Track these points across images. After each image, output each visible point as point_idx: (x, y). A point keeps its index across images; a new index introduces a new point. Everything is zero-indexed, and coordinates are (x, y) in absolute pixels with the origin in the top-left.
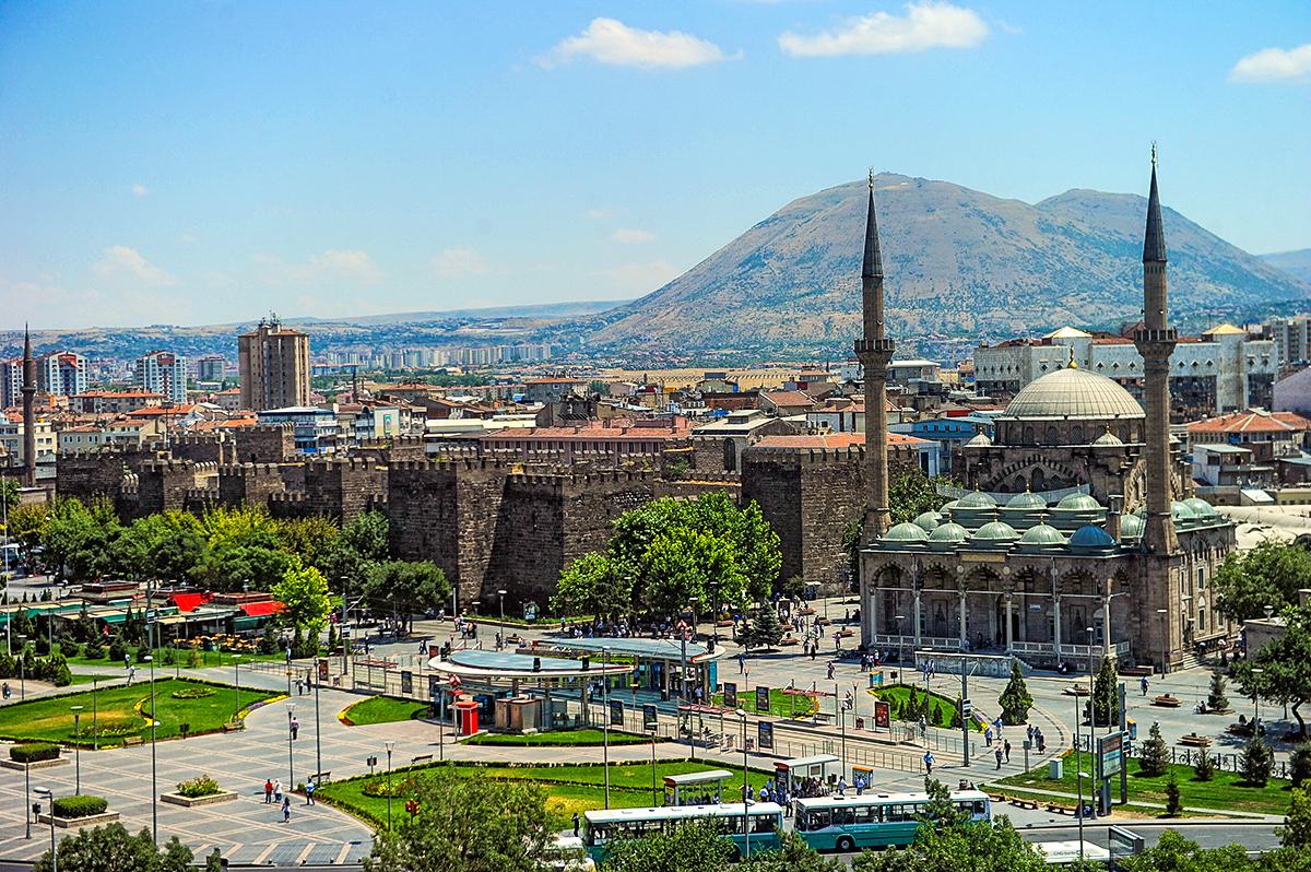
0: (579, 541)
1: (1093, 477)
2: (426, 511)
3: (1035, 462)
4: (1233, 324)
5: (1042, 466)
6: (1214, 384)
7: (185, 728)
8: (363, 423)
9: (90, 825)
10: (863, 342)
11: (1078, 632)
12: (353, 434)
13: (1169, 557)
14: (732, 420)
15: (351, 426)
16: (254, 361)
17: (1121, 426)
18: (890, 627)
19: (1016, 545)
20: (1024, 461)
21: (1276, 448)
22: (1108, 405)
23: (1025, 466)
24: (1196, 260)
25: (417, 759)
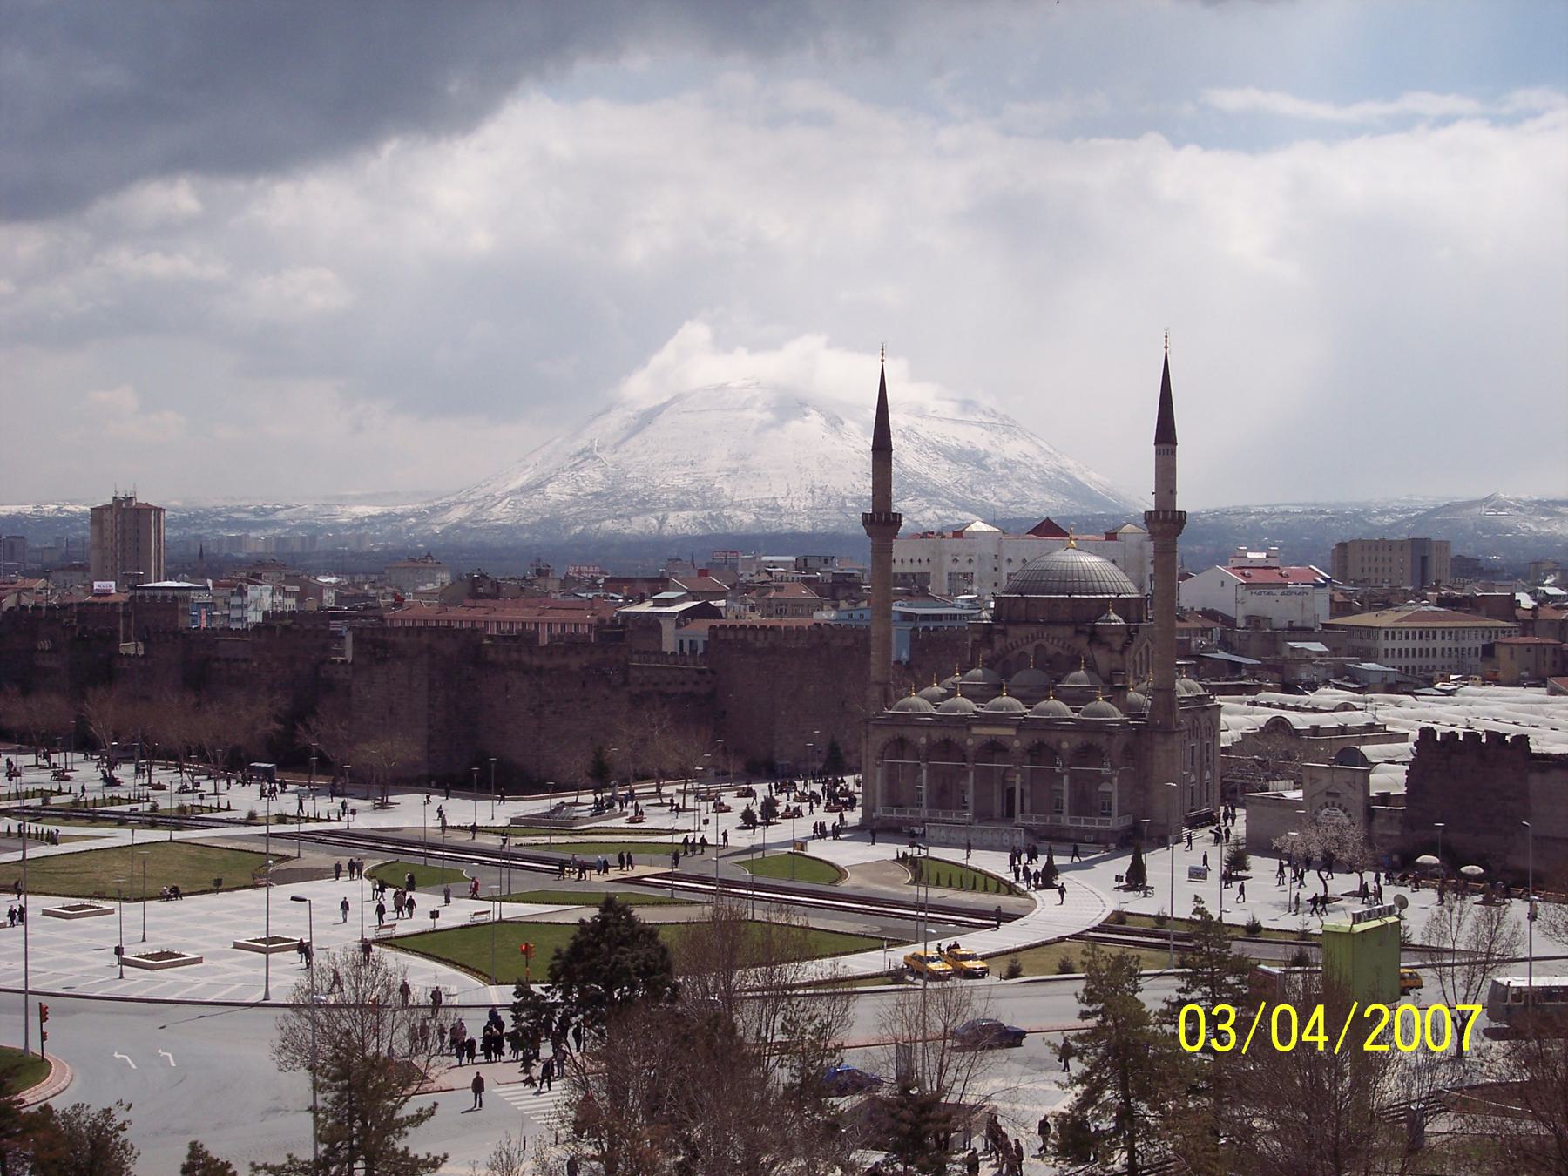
0: (554, 713)
1: (1095, 654)
2: (394, 679)
3: (1038, 638)
4: (523, 639)
5: (1046, 643)
6: (867, 639)
7: (218, 882)
8: (236, 600)
9: (1480, 651)
10: (242, 619)
11: (1085, 803)
12: (227, 612)
13: (1175, 732)
14: (659, 603)
15: (225, 603)
16: (107, 534)
17: (1122, 605)
18: (893, 801)
19: (1025, 719)
20: (1027, 638)
21: (1193, 644)
22: (1108, 584)
23: (1028, 642)
24: (1031, 469)
25: (476, 914)
